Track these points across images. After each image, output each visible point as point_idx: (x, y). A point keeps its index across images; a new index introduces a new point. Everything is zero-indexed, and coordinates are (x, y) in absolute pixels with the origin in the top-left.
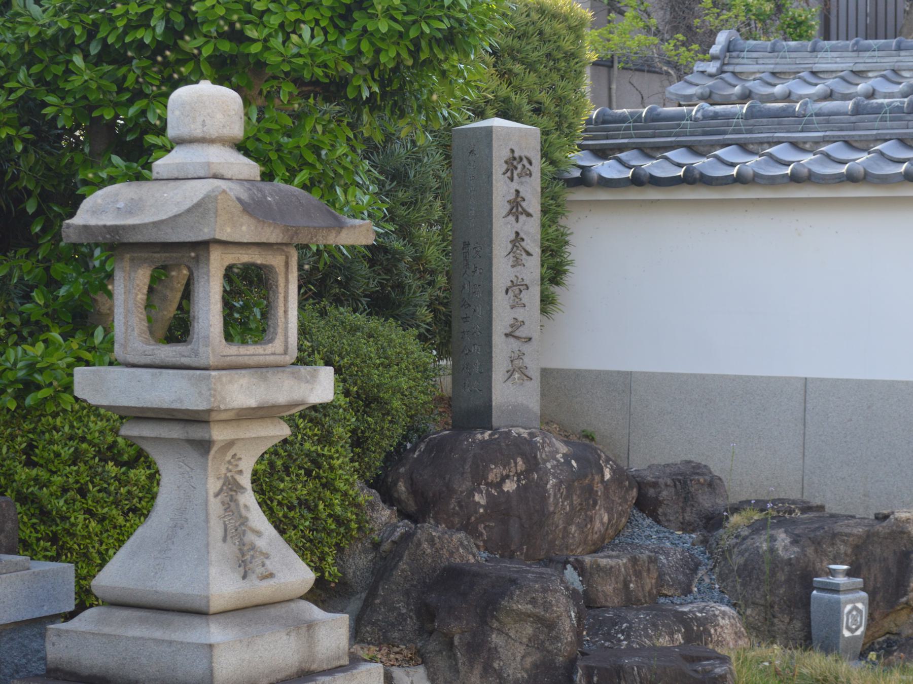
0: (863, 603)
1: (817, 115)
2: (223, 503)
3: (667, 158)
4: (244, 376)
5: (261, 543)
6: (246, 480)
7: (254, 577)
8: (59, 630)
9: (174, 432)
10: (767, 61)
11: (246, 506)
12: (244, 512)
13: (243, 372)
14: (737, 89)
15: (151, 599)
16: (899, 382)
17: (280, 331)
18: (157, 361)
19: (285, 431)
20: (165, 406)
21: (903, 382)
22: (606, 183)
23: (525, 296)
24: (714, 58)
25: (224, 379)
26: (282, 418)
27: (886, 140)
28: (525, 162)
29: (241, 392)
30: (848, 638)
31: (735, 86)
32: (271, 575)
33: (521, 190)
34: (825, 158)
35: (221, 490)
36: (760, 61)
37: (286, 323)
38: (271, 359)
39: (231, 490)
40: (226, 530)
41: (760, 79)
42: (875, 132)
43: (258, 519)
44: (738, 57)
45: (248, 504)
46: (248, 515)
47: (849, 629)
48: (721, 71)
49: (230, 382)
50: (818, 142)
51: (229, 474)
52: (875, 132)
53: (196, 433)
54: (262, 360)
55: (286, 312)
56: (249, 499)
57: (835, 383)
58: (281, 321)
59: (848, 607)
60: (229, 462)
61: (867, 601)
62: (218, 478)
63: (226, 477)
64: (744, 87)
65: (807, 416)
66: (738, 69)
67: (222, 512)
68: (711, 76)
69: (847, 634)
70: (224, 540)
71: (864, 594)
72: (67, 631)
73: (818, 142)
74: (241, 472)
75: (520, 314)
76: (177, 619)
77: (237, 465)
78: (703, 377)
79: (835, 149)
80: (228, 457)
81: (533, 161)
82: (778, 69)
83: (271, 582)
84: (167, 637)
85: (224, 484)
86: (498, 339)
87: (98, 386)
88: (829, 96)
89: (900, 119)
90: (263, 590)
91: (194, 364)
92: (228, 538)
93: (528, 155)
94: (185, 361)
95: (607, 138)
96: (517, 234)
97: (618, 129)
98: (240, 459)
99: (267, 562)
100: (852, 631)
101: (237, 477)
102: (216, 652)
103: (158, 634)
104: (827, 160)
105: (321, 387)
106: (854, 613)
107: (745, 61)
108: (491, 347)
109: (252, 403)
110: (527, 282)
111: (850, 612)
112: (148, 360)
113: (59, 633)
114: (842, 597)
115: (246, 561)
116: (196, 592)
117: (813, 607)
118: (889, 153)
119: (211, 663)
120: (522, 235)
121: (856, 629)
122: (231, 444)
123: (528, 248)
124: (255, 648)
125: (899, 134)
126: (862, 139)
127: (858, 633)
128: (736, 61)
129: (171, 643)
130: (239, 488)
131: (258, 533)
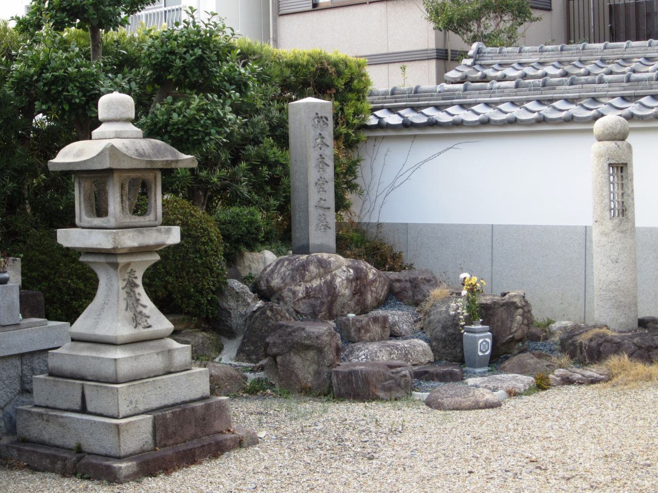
0: (490, 339)
1: (498, 88)
2: (127, 292)
3: (422, 113)
4: (130, 232)
5: (146, 311)
6: (139, 281)
7: (141, 327)
8: (53, 353)
9: (102, 259)
10: (497, 58)
11: (139, 294)
12: (138, 297)
13: (130, 230)
14: (479, 74)
15: (93, 338)
16: (537, 226)
17: (153, 210)
18: (93, 226)
19: (157, 258)
20: (95, 247)
21: (540, 226)
22: (389, 127)
23: (326, 187)
24: (470, 57)
25: (120, 234)
26: (156, 251)
27: (531, 101)
28: (324, 119)
29: (130, 240)
30: (481, 356)
31: (478, 71)
32: (150, 327)
33: (322, 133)
34: (610, 107)
35: (126, 286)
36: (494, 58)
37: (156, 206)
38: (148, 223)
39: (132, 286)
40: (127, 305)
41: (595, 63)
42: (525, 97)
43: (145, 299)
44: (483, 56)
45: (140, 293)
46: (140, 298)
47: (481, 351)
48: (474, 64)
49: (123, 235)
50: (497, 103)
51: (130, 279)
52: (525, 97)
53: (111, 260)
54: (143, 224)
55: (155, 201)
56: (141, 290)
57: (507, 227)
58: (153, 205)
59: (481, 341)
60: (130, 273)
61: (491, 337)
62: (124, 280)
63: (129, 280)
64: (483, 73)
65: (494, 244)
66: (483, 62)
67: (126, 297)
68: (469, 66)
69: (480, 354)
70: (126, 310)
71: (489, 333)
72: (56, 353)
73: (497, 103)
74: (136, 278)
75: (324, 196)
76: (103, 347)
77: (134, 275)
78: (443, 225)
79: (531, 105)
80: (129, 270)
81: (329, 119)
82: (542, 60)
83: (150, 329)
84: (98, 356)
85: (127, 283)
86: (312, 209)
87: (67, 238)
88: (588, 74)
89: (538, 90)
90: (142, 332)
91: (108, 227)
92: (129, 309)
93: (326, 116)
94: (105, 225)
95: (396, 102)
96: (321, 155)
97: (403, 97)
98: (135, 271)
99: (148, 320)
100: (483, 352)
101: (134, 280)
102: (118, 362)
103: (94, 354)
104: (499, 112)
105: (174, 236)
106: (484, 343)
107: (486, 58)
108: (308, 213)
109: (136, 244)
110: (327, 180)
111: (482, 343)
112: (89, 225)
113: (53, 354)
114: (477, 335)
115: (137, 318)
116: (111, 335)
117: (464, 340)
118: (586, 105)
119: (116, 367)
120: (323, 156)
121: (486, 351)
122: (128, 264)
123: (327, 163)
124: (139, 360)
125: (623, 94)
126: (519, 101)
127: (487, 353)
128: (482, 58)
129: (99, 358)
130: (137, 286)
131: (145, 307)
